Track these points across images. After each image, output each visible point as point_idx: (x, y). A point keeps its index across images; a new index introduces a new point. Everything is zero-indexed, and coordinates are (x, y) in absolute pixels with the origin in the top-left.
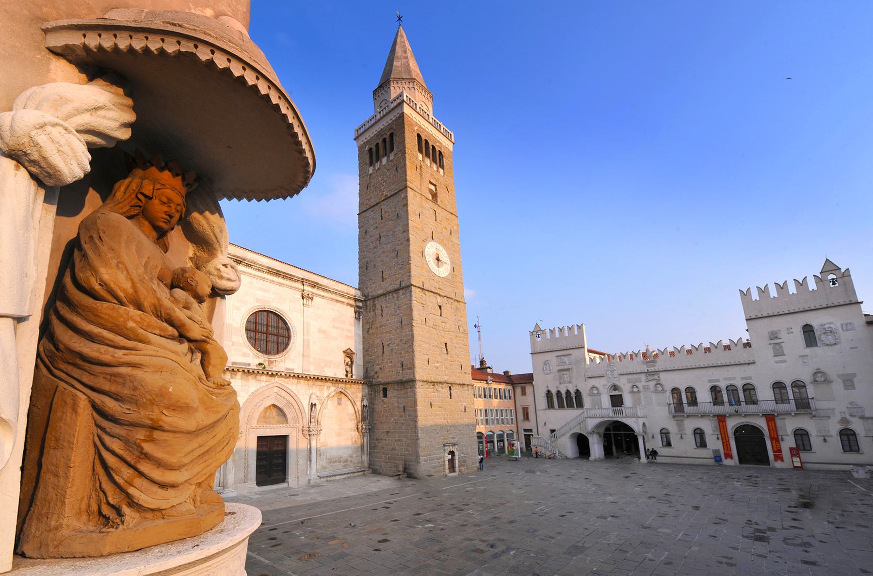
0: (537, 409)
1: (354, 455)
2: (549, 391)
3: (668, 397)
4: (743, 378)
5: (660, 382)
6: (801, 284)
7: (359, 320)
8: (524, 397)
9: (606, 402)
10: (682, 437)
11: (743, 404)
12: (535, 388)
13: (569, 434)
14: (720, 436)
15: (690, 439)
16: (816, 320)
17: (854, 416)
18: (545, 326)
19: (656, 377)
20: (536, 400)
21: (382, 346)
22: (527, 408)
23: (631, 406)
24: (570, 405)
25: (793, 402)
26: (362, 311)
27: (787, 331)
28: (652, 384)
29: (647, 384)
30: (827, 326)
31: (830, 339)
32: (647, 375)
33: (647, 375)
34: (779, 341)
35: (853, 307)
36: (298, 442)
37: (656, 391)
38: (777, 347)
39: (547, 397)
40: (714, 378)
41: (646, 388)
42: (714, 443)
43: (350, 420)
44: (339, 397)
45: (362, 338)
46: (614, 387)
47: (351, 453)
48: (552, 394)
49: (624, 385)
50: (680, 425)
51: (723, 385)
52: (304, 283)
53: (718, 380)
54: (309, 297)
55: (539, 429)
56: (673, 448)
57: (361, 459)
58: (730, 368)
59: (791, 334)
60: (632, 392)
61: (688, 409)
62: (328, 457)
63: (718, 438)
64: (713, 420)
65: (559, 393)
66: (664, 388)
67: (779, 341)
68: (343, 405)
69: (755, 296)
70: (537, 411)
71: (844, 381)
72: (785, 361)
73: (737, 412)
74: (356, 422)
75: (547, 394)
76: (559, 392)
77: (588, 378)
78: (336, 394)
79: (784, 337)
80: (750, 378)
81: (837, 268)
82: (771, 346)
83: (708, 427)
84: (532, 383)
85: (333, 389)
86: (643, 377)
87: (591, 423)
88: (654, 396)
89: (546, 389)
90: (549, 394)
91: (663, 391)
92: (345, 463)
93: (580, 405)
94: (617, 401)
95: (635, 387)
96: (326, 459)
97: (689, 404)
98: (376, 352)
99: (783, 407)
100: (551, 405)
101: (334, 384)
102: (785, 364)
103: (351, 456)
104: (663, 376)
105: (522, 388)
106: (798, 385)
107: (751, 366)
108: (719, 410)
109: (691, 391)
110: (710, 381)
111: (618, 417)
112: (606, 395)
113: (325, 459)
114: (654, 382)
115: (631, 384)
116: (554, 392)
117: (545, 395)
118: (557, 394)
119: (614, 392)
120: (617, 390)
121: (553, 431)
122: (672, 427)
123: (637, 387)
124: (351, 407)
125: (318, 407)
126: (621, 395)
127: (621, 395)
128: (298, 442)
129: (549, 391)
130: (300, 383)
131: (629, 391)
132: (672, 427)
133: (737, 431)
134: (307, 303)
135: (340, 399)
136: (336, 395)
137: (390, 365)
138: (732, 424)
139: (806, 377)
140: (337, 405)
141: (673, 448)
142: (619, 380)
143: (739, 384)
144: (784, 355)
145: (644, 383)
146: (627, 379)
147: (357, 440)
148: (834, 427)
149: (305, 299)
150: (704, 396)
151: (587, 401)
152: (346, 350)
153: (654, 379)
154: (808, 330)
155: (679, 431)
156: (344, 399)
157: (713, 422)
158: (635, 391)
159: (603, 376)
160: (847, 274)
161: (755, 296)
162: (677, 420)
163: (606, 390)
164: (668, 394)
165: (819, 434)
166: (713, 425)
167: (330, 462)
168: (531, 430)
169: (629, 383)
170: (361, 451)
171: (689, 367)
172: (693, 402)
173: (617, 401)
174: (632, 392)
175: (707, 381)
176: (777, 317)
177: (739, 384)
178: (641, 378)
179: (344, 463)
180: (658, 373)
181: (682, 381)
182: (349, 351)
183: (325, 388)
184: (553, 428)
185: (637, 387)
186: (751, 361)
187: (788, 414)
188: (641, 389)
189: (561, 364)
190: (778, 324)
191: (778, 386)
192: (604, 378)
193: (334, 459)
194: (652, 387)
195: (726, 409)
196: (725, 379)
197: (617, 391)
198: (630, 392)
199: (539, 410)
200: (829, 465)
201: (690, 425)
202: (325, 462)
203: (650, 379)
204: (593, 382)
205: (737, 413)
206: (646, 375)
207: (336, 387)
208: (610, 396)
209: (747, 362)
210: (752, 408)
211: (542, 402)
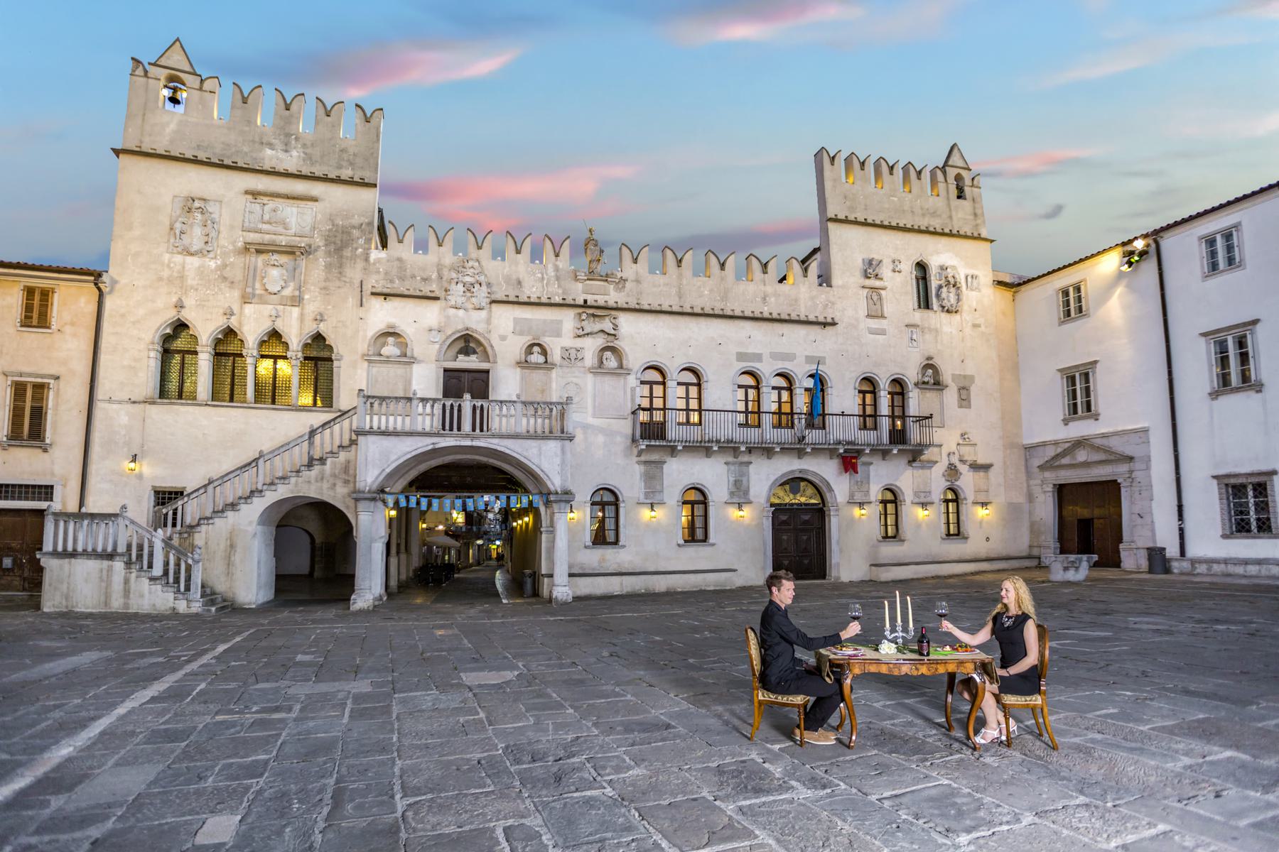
0: (100, 394)
2: (180, 327)
3: (631, 391)
5: (617, 344)
8: (34, 337)
9: (426, 380)
11: (767, 420)
12: (109, 303)
13: (259, 505)
19: (607, 325)
22: (40, 388)
25: (885, 424)
27: (891, 267)
28: (591, 346)
29: (579, 343)
32: (584, 316)
33: (584, 316)
34: (877, 283)
36: (127, 593)
38: (744, 468)
39: (166, 353)
40: (750, 350)
41: (571, 357)
46: (461, 344)
53: (758, 358)
56: (624, 546)
58: (786, 328)
59: (897, 273)
60: (524, 364)
64: (734, 464)
66: (624, 362)
67: (877, 283)
76: (229, 333)
77: (373, 294)
81: (966, 166)
86: (568, 319)
89: (171, 315)
91: (621, 370)
95: (536, 349)
99: (870, 436)
102: (884, 337)
104: (626, 323)
105: (30, 292)
107: (829, 328)
110: (741, 357)
112: (433, 366)
114: (600, 341)
115: (526, 340)
116: (205, 329)
117: (157, 339)
118: (218, 342)
121: (166, 497)
122: (629, 481)
126: (487, 372)
128: (127, 593)
129: (180, 327)
131: (518, 359)
132: (629, 481)
139: (911, 375)
141: (713, 545)
142: (488, 321)
144: (882, 317)
145: (567, 340)
146: (516, 321)
153: (603, 331)
155: (647, 495)
157: (732, 468)
159: (437, 298)
162: (646, 462)
163: (437, 346)
165: (917, 500)
168: (46, 492)
169: (521, 333)
171: (697, 310)
174: (524, 364)
175: (735, 357)
176: (687, 319)
177: (801, 371)
178: (561, 322)
180: (613, 313)
185: (544, 352)
186: (829, 320)
188: (556, 356)
189: (265, 227)
191: (869, 385)
194: (590, 359)
196: (776, 356)
197: (473, 357)
199: (110, 400)
200: (596, 578)
203: (588, 330)
204: (382, 314)
206: (580, 315)
208: (446, 370)
209: (821, 319)
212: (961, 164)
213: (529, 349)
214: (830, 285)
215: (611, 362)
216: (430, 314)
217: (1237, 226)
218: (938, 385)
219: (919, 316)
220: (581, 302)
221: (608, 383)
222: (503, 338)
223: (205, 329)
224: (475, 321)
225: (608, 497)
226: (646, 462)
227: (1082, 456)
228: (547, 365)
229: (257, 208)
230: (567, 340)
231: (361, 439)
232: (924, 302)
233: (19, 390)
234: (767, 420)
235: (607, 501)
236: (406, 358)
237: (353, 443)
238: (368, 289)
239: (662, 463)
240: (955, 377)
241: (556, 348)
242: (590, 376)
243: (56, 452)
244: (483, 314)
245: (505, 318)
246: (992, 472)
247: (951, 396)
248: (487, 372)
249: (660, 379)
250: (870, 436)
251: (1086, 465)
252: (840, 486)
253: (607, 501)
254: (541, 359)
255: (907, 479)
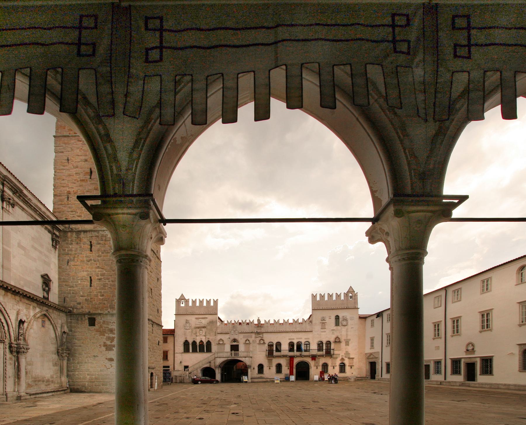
0: (176, 352)
1: (55, 377)
3: (266, 347)
4: (305, 339)
6: (338, 296)
7: (56, 250)
8: (165, 344)
9: (228, 348)
10: (270, 368)
11: (295, 351)
14: (289, 367)
15: (274, 369)
16: (342, 314)
17: (346, 357)
18: (188, 296)
19: (261, 336)
20: (175, 347)
21: (89, 279)
23: (244, 351)
24: (202, 350)
25: (324, 351)
26: (59, 240)
29: (255, 339)
30: (345, 317)
31: (344, 323)
35: (355, 310)
37: (260, 344)
38: (323, 324)
41: (254, 342)
42: (285, 370)
43: (52, 344)
44: (43, 320)
45: (57, 267)
46: (234, 340)
47: (52, 374)
48: (189, 343)
49: (241, 339)
50: (270, 362)
51: (295, 342)
52: (5, 182)
53: (293, 339)
54: (9, 202)
55: (176, 365)
57: (60, 380)
58: (300, 333)
60: (245, 343)
61: (275, 353)
62: (34, 376)
63: (288, 368)
65: (194, 343)
68: (46, 328)
69: (318, 298)
70: (176, 355)
71: (346, 342)
72: (325, 332)
73: (301, 355)
74: (56, 346)
75: (184, 343)
76: (201, 341)
78: (41, 316)
79: (327, 320)
80: (309, 339)
82: (321, 324)
83: (284, 362)
84: (174, 335)
85: (38, 310)
86: (253, 335)
87: (219, 361)
88: (258, 346)
89: (185, 339)
90: (186, 343)
92: (48, 383)
93: (209, 350)
94: (235, 348)
96: (32, 377)
97: (454, 321)
98: (80, 284)
99: (320, 353)
100: (186, 350)
101: (39, 306)
103: (52, 377)
104: (265, 335)
106: (329, 343)
108: (291, 354)
109: (279, 344)
110: (289, 339)
111: (238, 357)
113: (30, 377)
114: (260, 338)
115: (246, 339)
116: (191, 342)
119: (234, 343)
120: (236, 342)
123: (249, 341)
124: (52, 331)
125: (26, 325)
126: (238, 345)
127: (238, 345)
130: (7, 295)
133: (299, 364)
134: (8, 209)
135: (43, 322)
136: (40, 317)
137: (101, 298)
138: (296, 361)
139: (332, 340)
140: (41, 327)
143: (295, 342)
146: (244, 336)
147: (57, 362)
148: (338, 362)
149: (5, 203)
150: (285, 347)
151: (214, 348)
152: (44, 275)
154: (337, 318)
156: (47, 323)
158: (247, 343)
160: (356, 295)
161: (318, 298)
164: (266, 345)
166: (287, 362)
167: (35, 381)
168: (168, 367)
170: (60, 373)
172: (278, 350)
173: (235, 348)
174: (245, 343)
179: (46, 382)
181: (274, 339)
182: (46, 277)
183: (31, 307)
184: (186, 365)
185: (249, 341)
186: (311, 331)
187: (322, 356)
188: (251, 341)
190: (326, 314)
192: (229, 335)
193: (38, 378)
194: (258, 342)
195: (295, 353)
196: (297, 339)
198: (244, 343)
201: (275, 361)
202: (30, 380)
204: (219, 337)
205: (301, 356)
207: (40, 308)
210: (307, 353)
211: (180, 348)
212: (352, 291)
213: (246, 341)
214: (312, 295)
215: (262, 342)
216: (227, 336)
217: (460, 289)
218: (340, 342)
219: (335, 328)
220: (256, 332)
221: (262, 346)
222: (241, 339)
223: (191, 342)
224: (236, 337)
225: (307, 343)
226: (269, 359)
227: (372, 356)
228: (249, 343)
229: (197, 321)
230: (253, 338)
231: (216, 359)
232: (337, 324)
233: (164, 352)
234: (295, 351)
235: (261, 368)
236: (224, 344)
237: (215, 359)
238: (216, 333)
239: (272, 359)
240: (344, 340)
241: (251, 340)
242: (258, 345)
243: (169, 361)
244: (237, 335)
245: (241, 336)
246: (354, 360)
247: (343, 344)
248: (238, 345)
249: (309, 343)
250: (320, 353)
251: (372, 358)
252: (312, 363)
253: (261, 368)
254: (248, 342)
255: (328, 361)
